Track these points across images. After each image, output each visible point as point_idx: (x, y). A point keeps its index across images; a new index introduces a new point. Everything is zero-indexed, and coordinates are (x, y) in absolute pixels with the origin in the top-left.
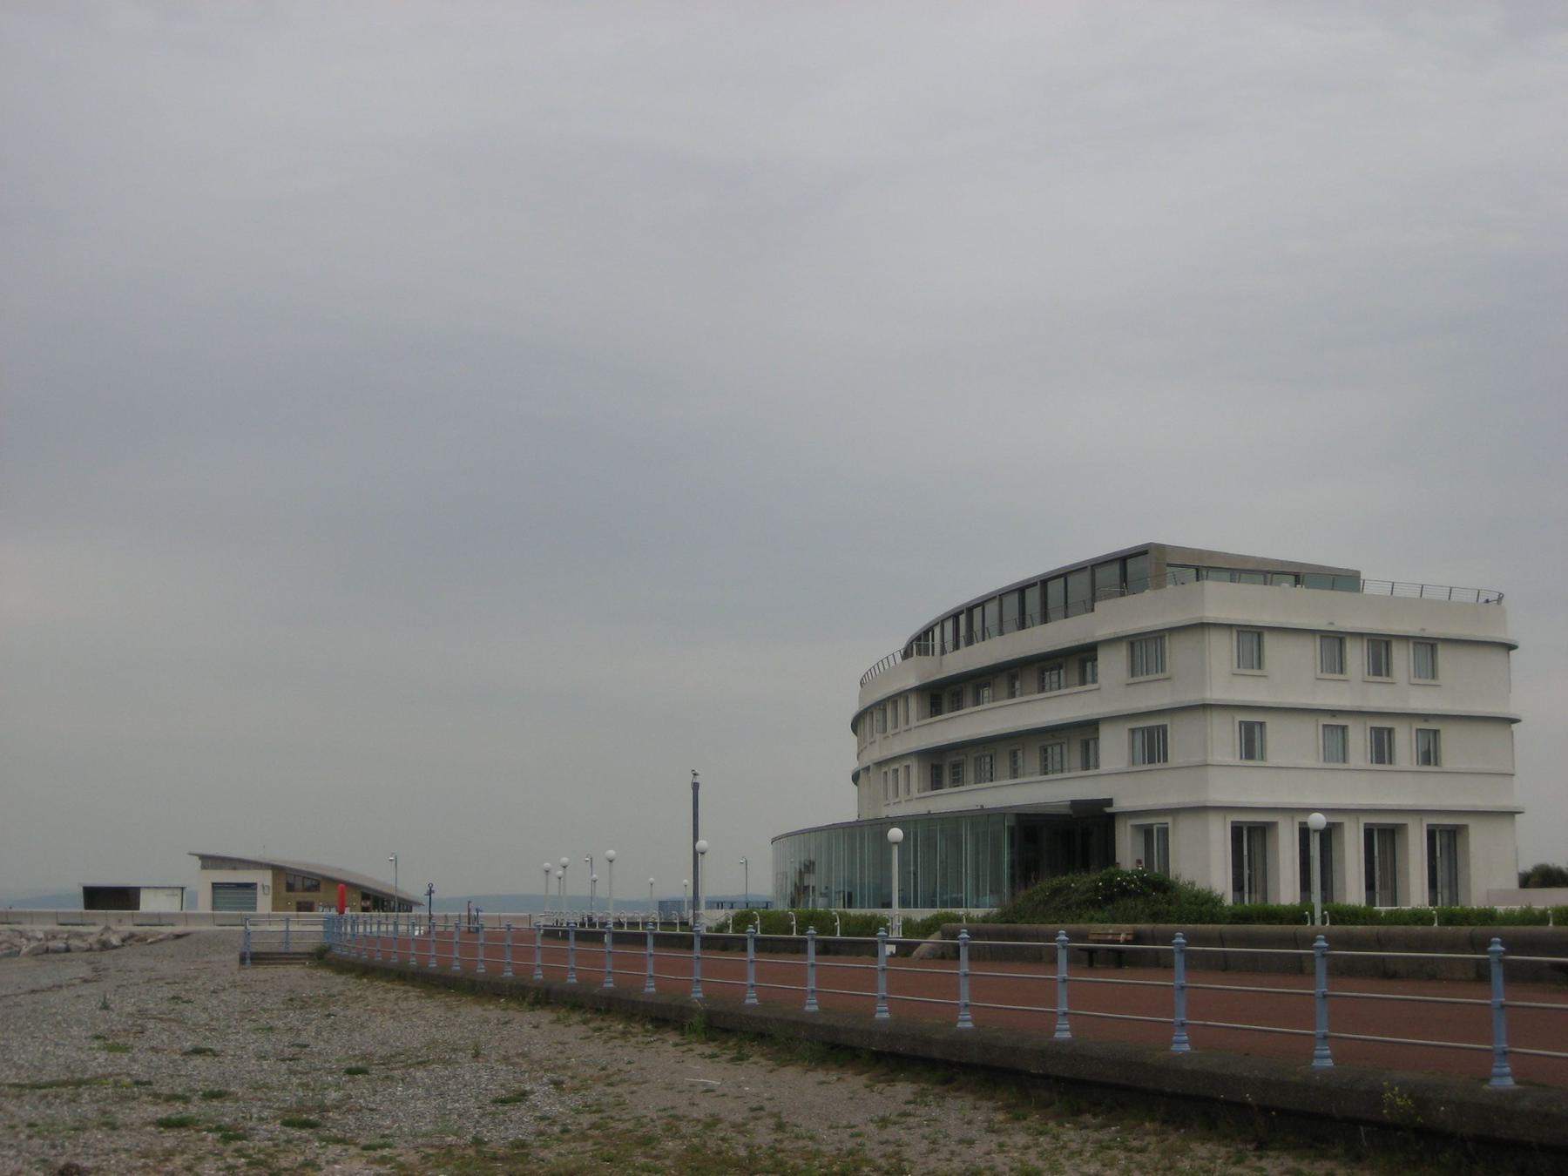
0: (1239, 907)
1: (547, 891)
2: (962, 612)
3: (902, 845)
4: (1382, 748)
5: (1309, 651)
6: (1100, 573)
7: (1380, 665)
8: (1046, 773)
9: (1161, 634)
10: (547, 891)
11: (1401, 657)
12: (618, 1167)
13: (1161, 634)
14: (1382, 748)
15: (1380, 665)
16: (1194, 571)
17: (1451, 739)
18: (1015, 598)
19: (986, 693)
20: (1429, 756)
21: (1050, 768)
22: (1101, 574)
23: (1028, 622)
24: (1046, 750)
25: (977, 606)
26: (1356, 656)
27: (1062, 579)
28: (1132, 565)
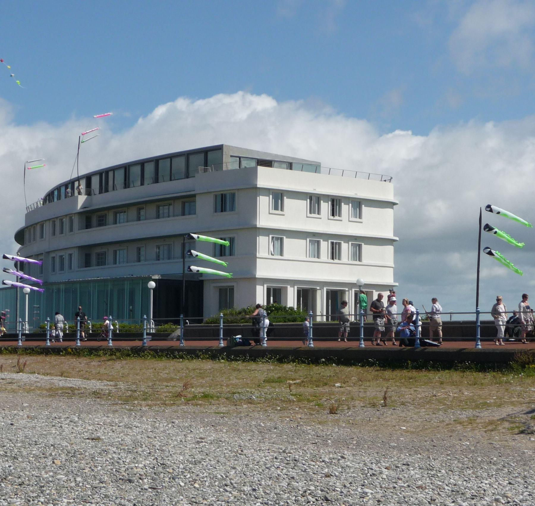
0: (328, 322)
1: (451, 320)
2: (69, 183)
3: (154, 290)
4: (335, 253)
5: (303, 205)
6: (192, 158)
7: (335, 211)
8: (159, 260)
9: (103, 213)
10: (451, 320)
11: (345, 208)
12: (83, 492)
13: (103, 213)
14: (335, 253)
15: (335, 211)
16: (238, 159)
17: (365, 248)
18: (122, 172)
19: (122, 217)
20: (358, 255)
21: (142, 258)
22: (175, 161)
23: (160, 179)
24: (140, 250)
25: (111, 170)
26: (325, 207)
27: (169, 159)
28: (210, 155)
